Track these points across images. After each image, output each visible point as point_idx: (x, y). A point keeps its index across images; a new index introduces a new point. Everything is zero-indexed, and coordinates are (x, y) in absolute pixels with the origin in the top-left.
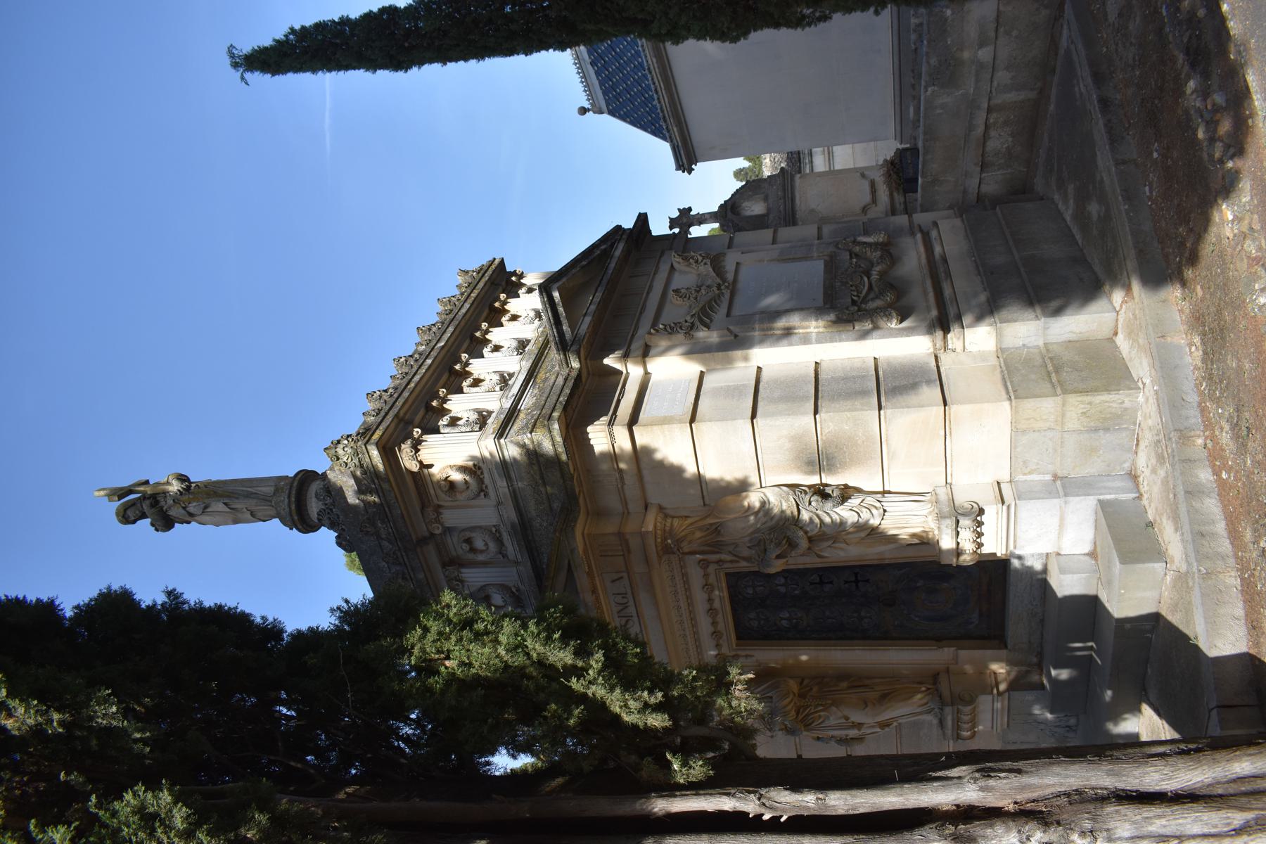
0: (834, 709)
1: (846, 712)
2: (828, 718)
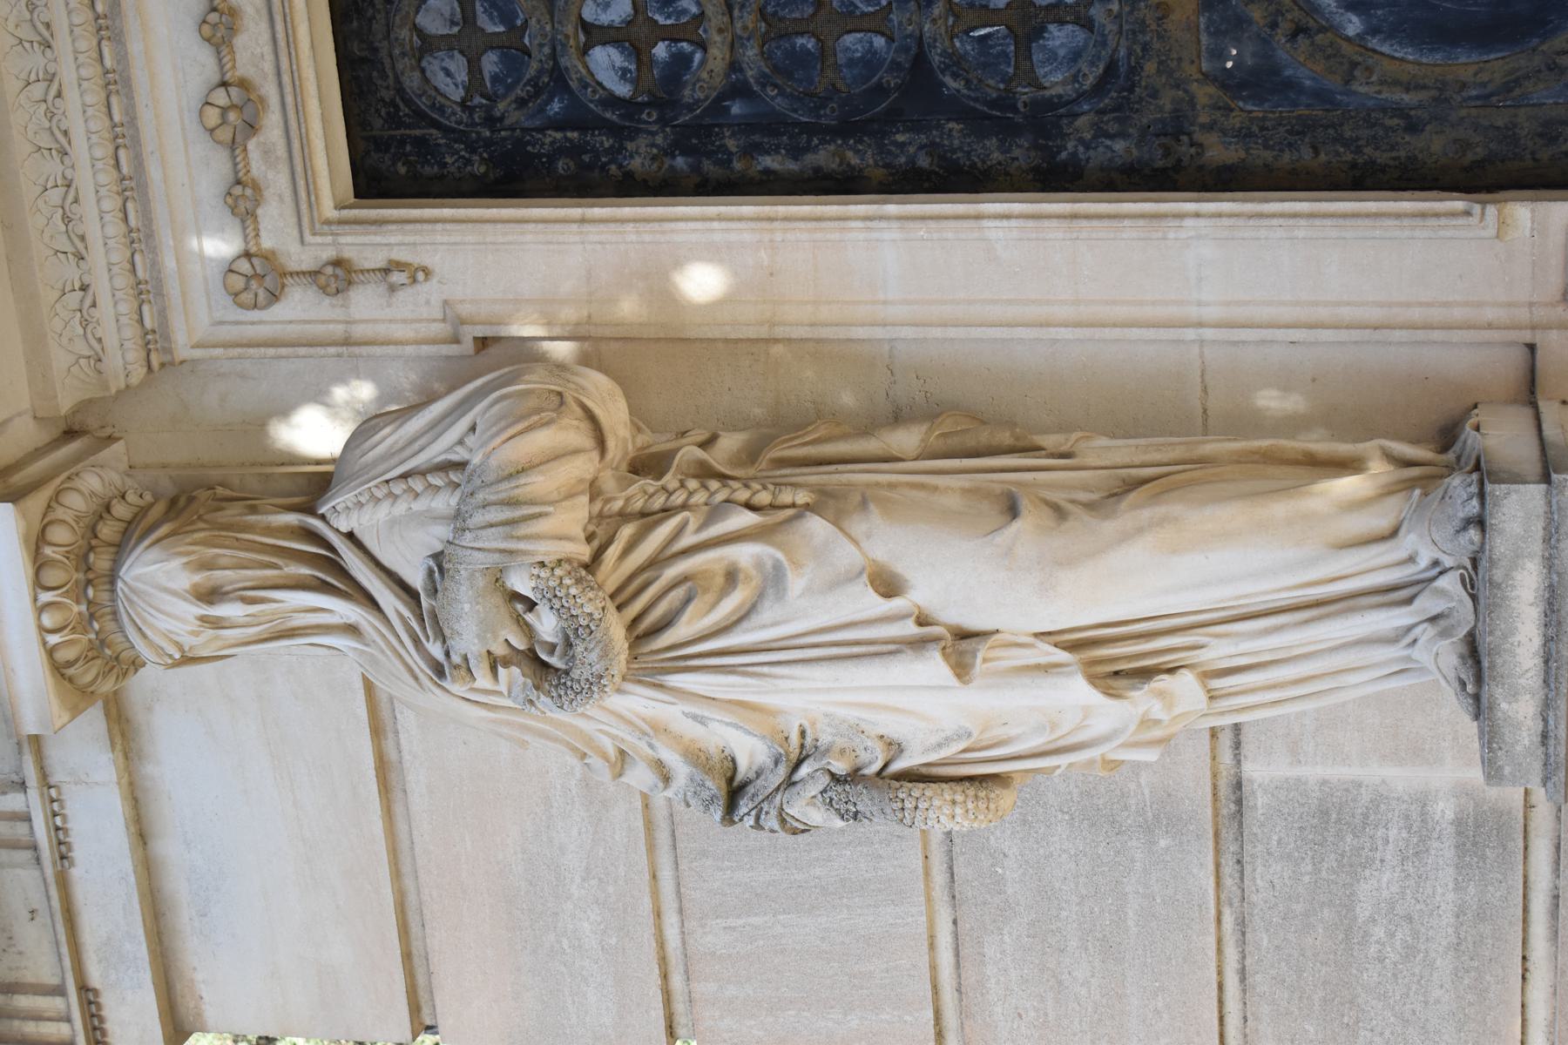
0: (817, 526)
1: (885, 540)
2: (774, 580)
